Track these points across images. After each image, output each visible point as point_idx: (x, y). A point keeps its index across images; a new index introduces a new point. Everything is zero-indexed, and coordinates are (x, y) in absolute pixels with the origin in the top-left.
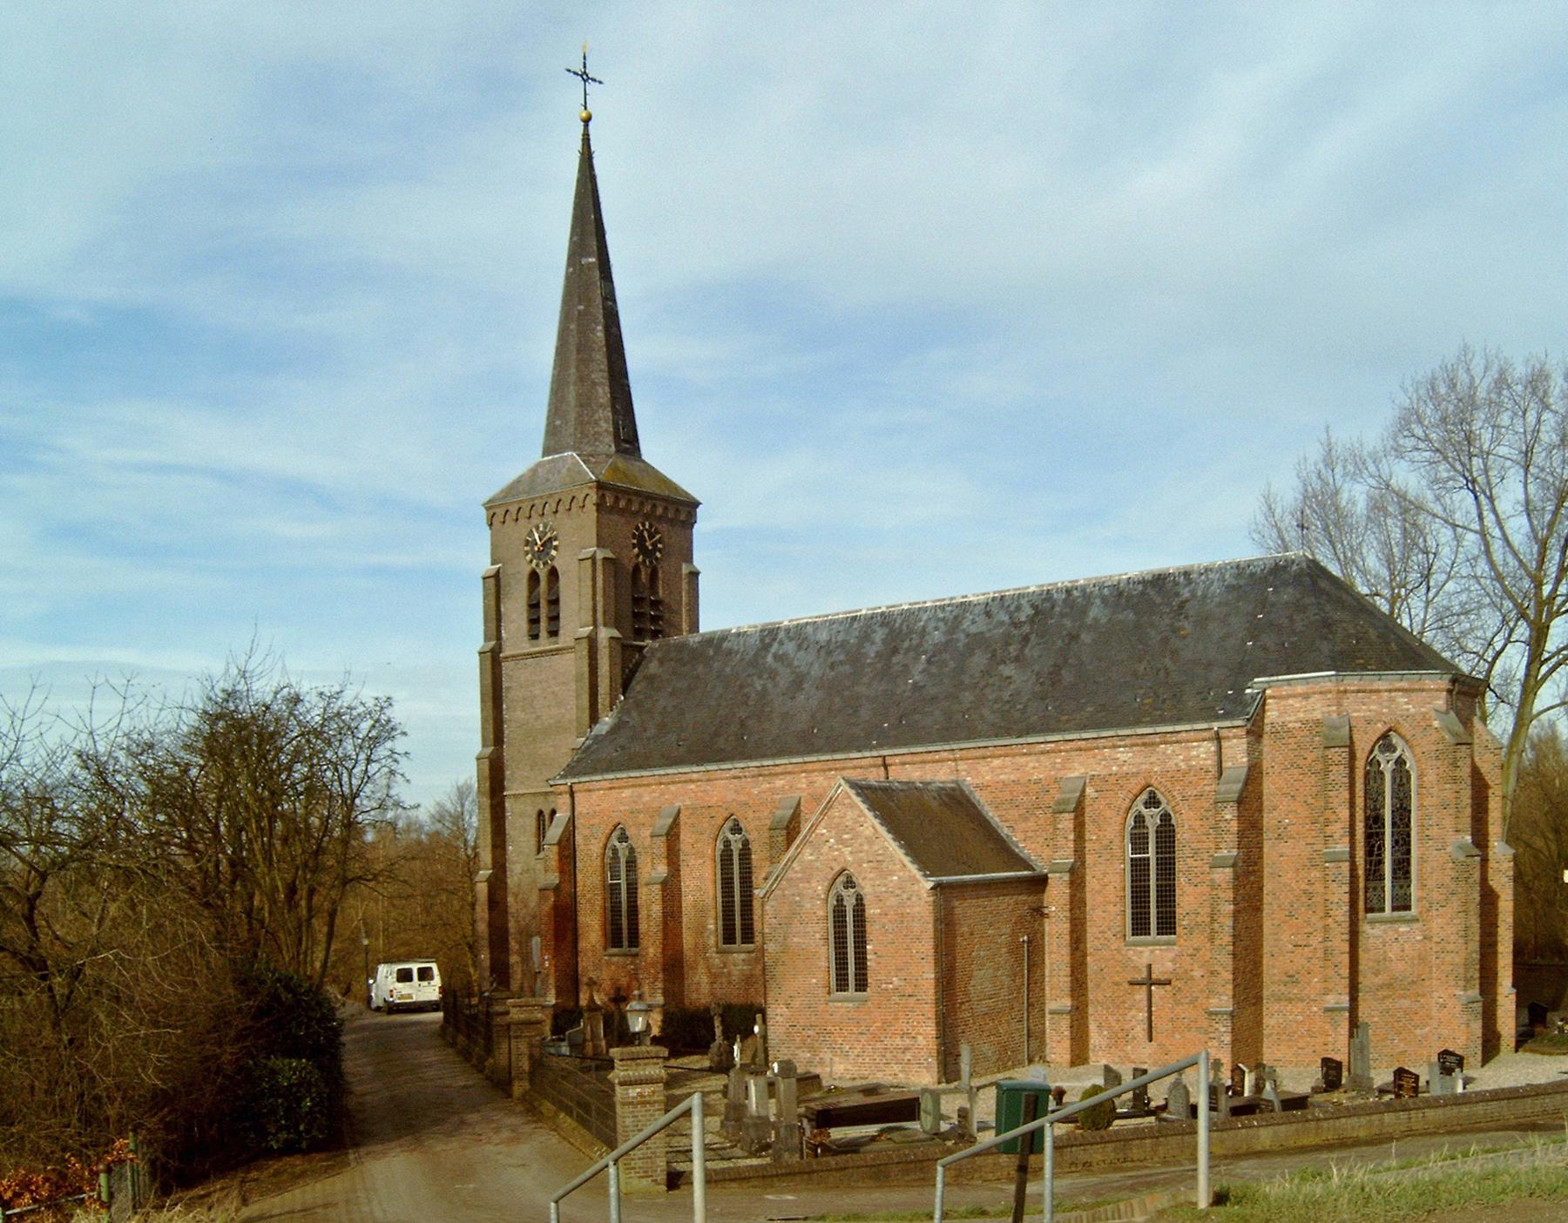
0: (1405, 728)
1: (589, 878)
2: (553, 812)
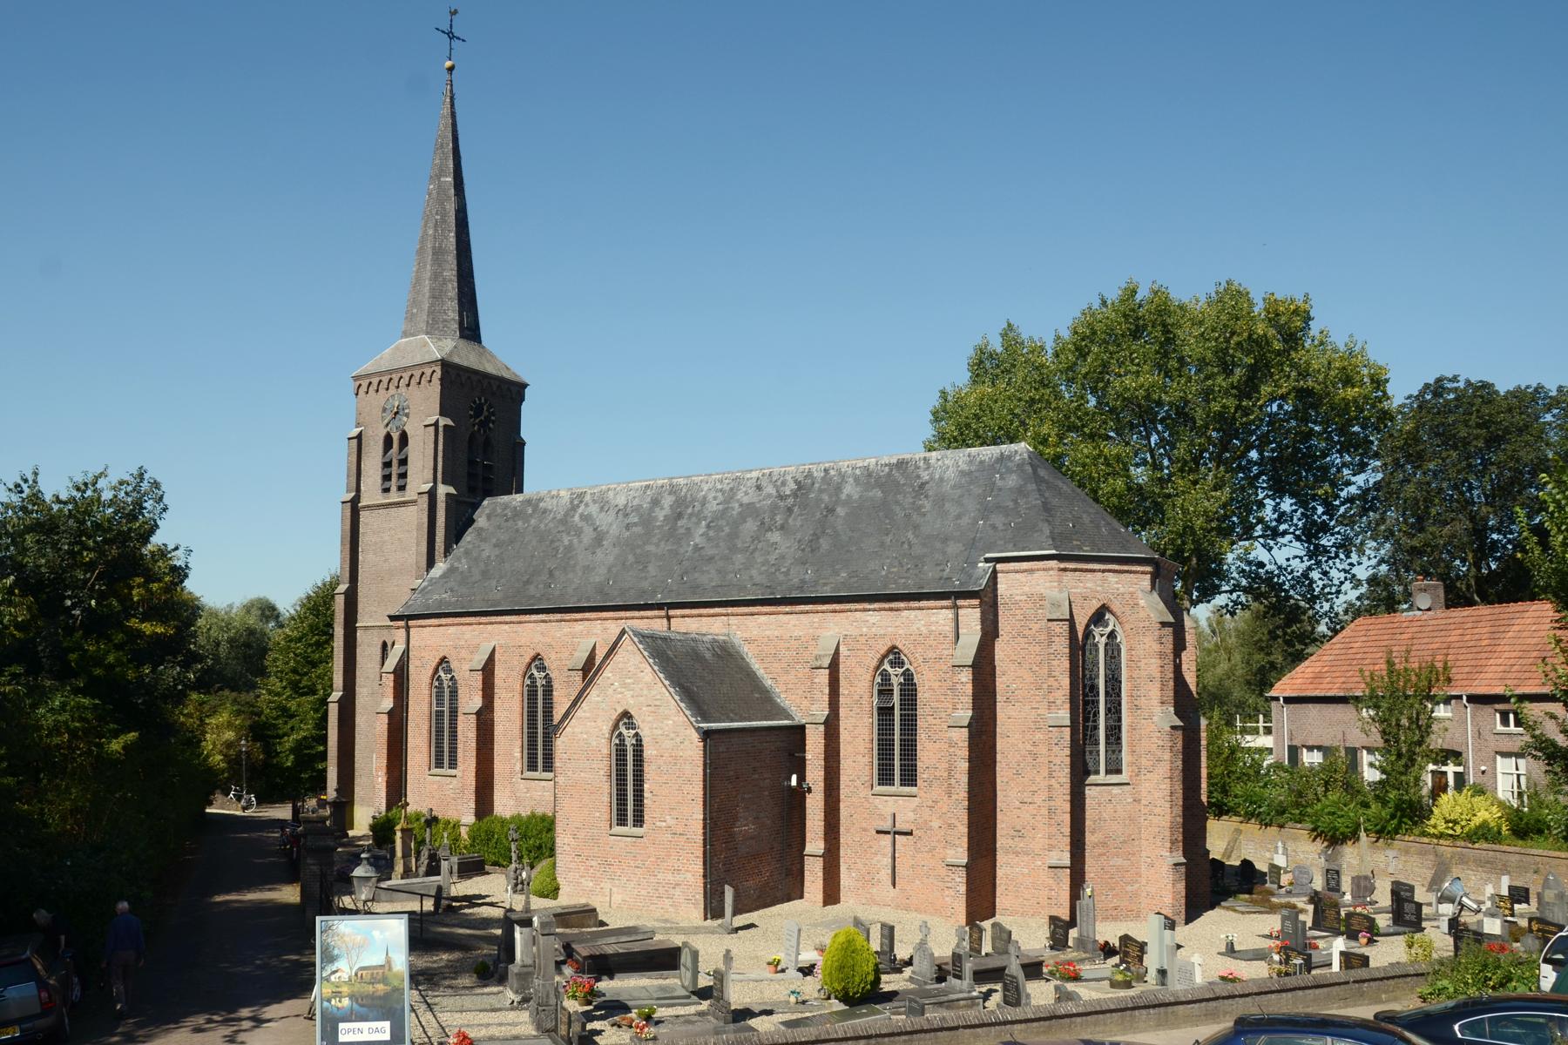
0: (1115, 607)
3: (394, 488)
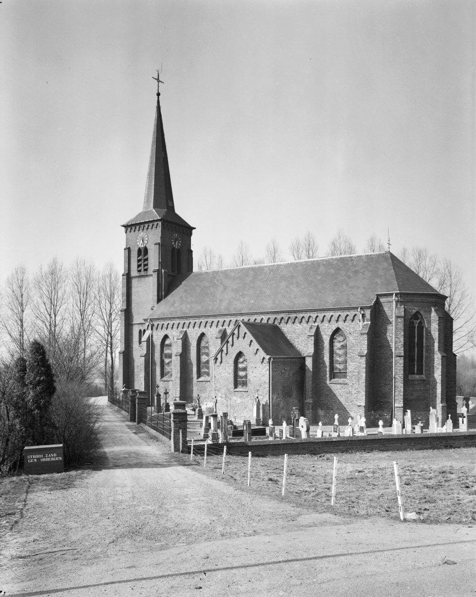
2: (145, 331)
3: (143, 270)
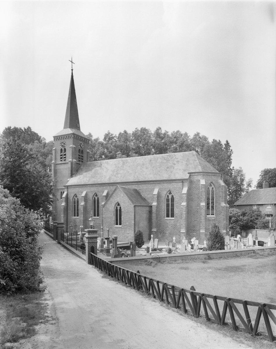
0: (214, 182)
1: (71, 204)
2: (64, 192)
3: (63, 160)
